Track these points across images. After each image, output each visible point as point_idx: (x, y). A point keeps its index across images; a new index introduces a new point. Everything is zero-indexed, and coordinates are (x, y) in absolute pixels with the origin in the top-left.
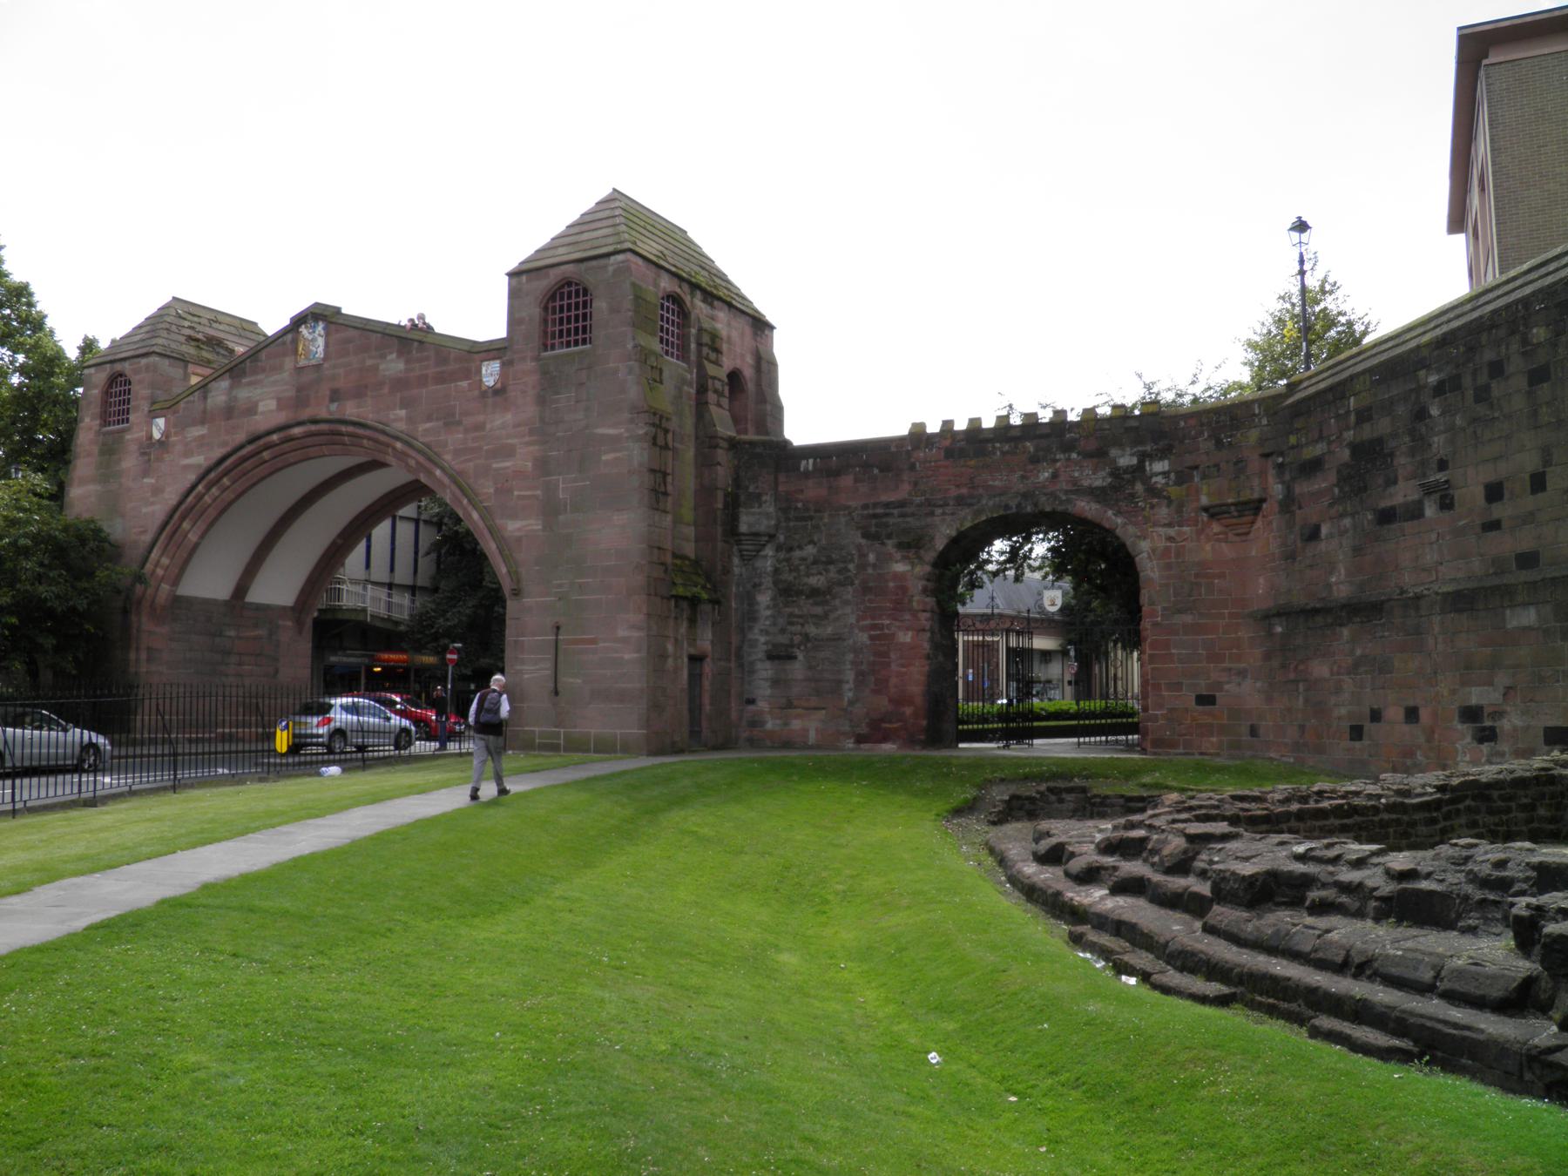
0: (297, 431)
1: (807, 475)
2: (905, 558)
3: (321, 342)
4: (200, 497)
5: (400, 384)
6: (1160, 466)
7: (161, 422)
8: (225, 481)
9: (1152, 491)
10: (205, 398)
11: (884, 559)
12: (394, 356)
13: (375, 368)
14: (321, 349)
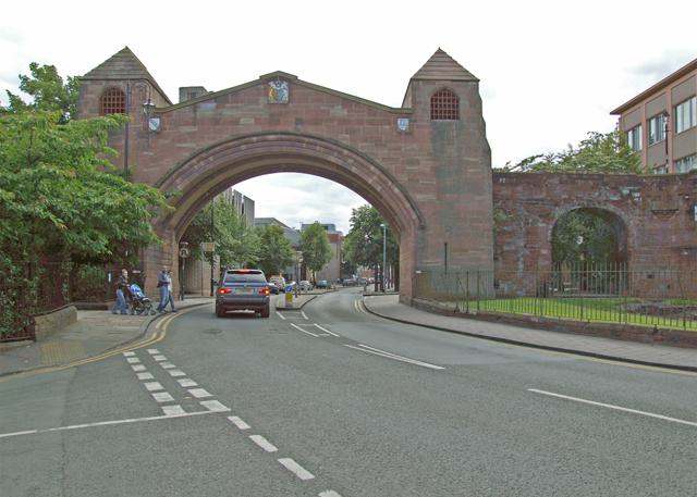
0: (271, 137)
1: (502, 184)
2: (543, 222)
3: (286, 92)
4: (192, 166)
5: (342, 121)
6: (637, 195)
7: (157, 121)
8: (211, 159)
9: (634, 203)
10: (195, 111)
11: (535, 221)
12: (340, 107)
13: (328, 111)
14: (287, 95)
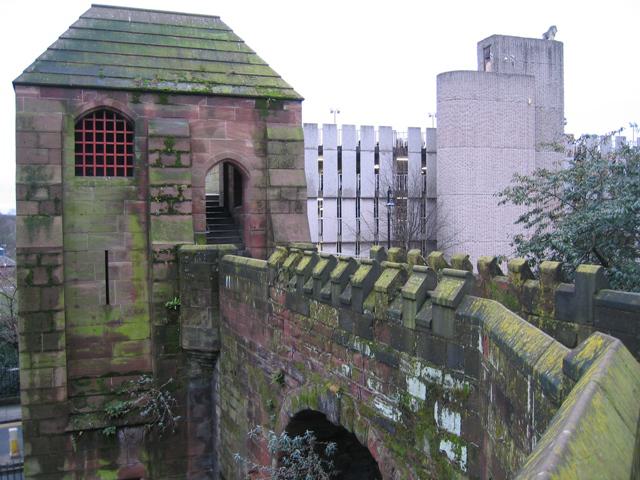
6: (452, 422)
